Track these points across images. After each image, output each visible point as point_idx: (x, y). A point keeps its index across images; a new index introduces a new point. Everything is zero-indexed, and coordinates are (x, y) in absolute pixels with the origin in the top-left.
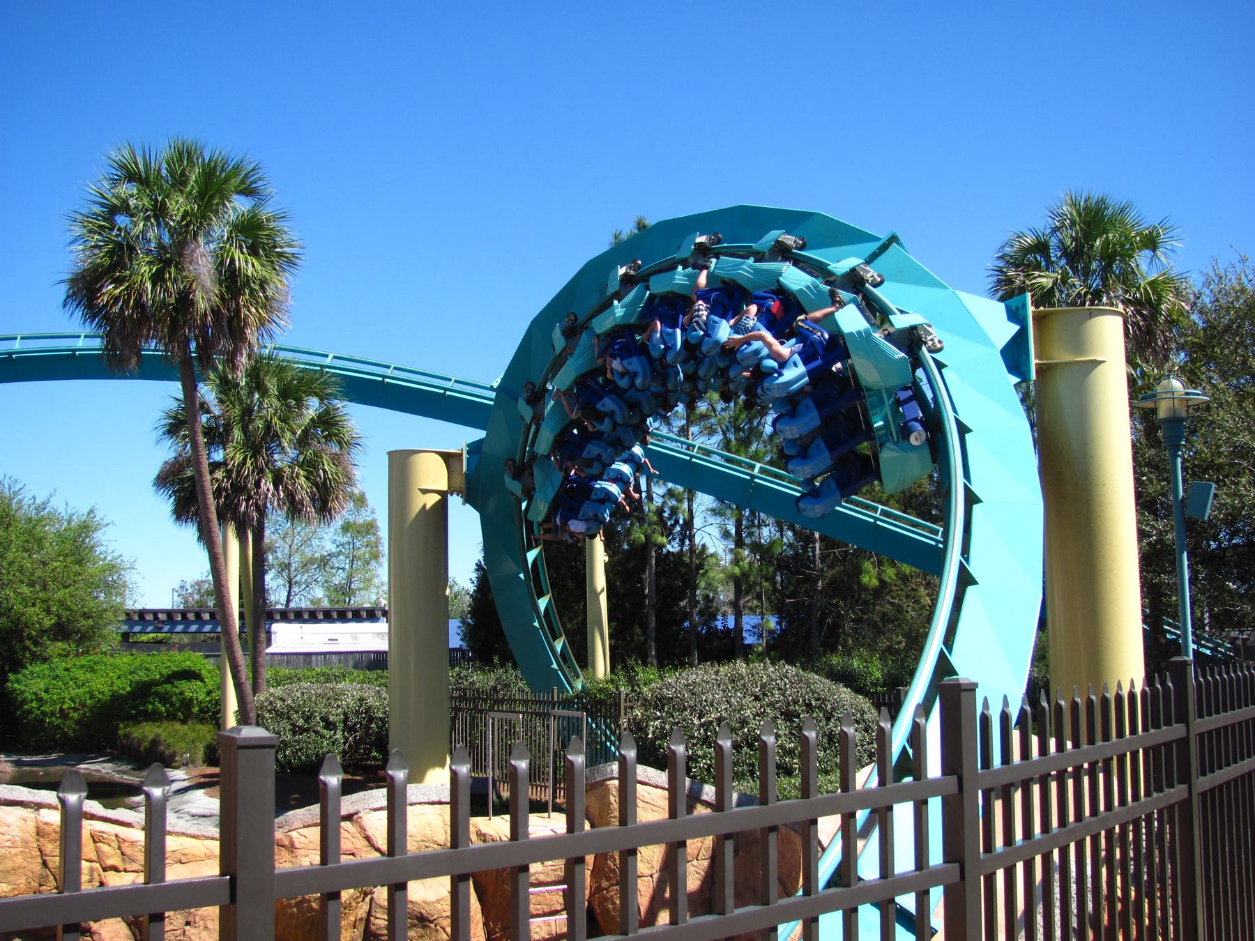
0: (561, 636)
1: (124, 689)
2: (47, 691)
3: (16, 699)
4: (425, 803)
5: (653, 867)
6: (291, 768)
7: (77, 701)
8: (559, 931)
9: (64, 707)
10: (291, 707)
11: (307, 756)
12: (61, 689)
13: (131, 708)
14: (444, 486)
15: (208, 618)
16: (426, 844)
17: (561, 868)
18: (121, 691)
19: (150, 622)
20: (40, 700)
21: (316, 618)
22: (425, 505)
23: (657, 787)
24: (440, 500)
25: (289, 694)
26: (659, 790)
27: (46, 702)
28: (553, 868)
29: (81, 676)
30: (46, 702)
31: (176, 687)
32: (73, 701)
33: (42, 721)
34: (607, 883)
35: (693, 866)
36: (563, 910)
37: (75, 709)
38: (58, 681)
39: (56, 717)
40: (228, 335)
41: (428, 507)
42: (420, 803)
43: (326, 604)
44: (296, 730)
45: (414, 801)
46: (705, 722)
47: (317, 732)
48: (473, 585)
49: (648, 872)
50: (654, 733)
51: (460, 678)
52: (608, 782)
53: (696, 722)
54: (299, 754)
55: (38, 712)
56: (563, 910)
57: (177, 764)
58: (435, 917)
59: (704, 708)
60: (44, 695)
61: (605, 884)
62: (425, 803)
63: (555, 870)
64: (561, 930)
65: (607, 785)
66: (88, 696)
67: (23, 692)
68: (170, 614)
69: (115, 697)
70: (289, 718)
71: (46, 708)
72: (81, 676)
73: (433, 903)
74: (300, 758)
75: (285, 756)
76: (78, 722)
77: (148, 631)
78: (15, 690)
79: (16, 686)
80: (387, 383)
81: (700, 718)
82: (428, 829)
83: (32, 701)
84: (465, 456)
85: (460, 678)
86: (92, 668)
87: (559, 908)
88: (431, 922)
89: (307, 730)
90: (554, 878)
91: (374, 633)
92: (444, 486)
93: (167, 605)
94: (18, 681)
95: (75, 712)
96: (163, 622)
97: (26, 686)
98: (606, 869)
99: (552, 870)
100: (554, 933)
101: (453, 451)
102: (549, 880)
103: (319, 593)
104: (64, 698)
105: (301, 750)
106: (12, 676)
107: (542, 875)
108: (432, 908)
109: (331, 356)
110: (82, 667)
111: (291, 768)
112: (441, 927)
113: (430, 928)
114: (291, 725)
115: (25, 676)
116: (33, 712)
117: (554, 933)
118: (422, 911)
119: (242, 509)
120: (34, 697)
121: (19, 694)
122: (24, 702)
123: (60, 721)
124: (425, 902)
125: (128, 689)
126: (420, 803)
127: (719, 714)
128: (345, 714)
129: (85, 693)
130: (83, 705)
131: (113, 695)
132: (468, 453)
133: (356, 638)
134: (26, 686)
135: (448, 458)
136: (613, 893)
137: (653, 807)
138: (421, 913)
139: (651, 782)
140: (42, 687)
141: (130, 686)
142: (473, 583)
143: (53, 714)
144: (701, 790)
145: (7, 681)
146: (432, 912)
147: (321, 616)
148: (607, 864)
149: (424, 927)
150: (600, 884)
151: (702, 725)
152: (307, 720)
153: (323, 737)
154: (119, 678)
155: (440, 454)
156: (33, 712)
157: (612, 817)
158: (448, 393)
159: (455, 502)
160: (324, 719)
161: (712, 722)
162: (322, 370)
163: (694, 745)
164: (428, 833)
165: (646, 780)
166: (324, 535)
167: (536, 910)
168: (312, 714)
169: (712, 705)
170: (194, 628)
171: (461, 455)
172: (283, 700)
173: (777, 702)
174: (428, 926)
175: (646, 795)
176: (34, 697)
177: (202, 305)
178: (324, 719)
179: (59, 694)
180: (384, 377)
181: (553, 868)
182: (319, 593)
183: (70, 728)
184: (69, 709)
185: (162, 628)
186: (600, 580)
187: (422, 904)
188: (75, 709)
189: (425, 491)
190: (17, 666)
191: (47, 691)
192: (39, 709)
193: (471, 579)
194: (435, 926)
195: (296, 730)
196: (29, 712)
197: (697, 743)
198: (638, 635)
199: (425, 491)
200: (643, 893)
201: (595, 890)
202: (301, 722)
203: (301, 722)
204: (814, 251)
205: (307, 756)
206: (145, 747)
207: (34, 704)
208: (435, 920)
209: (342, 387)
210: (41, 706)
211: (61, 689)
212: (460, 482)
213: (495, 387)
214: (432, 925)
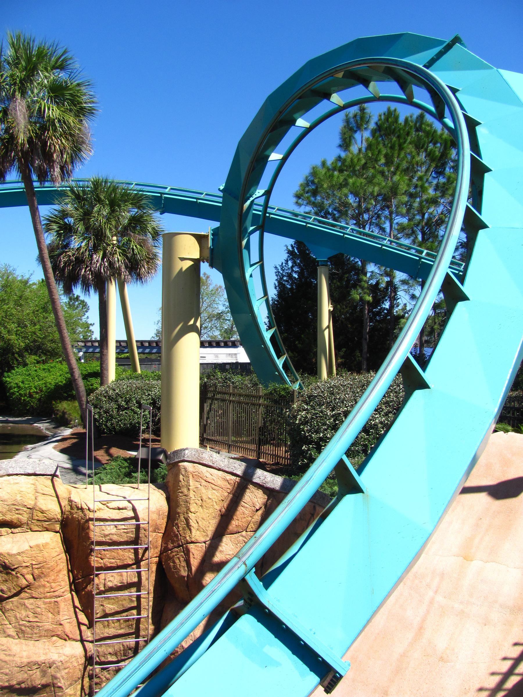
0: (285, 354)
1: (62, 382)
2: (23, 382)
3: (7, 387)
4: (22, 474)
5: (207, 536)
6: (115, 431)
7: (38, 388)
8: (130, 581)
9: (31, 391)
10: (119, 395)
11: (125, 424)
12: (30, 381)
13: (64, 392)
14: (197, 256)
15: (148, 345)
16: (17, 507)
17: (132, 531)
18: (60, 383)
19: (147, 348)
20: (19, 387)
21: (204, 345)
22: (181, 269)
23: (219, 470)
24: (192, 265)
25: (118, 387)
26: (221, 472)
27: (22, 389)
28: (126, 531)
29: (42, 374)
30: (22, 389)
31: (89, 382)
32: (36, 389)
33: (20, 399)
34: (172, 545)
35: (242, 536)
36: (133, 564)
37: (37, 393)
38: (29, 377)
39: (27, 397)
40: (41, 157)
41: (184, 269)
42: (17, 475)
43: (220, 338)
44: (120, 408)
45: (11, 473)
46: (335, 414)
47: (133, 410)
48: (266, 326)
49: (203, 539)
50: (300, 420)
51: (226, 379)
52: (180, 464)
53: (329, 413)
54: (120, 423)
55: (18, 394)
56: (133, 564)
57: (71, 426)
58: (16, 566)
59: (337, 404)
60: (21, 385)
61: (170, 546)
62: (22, 474)
63: (127, 533)
64: (131, 579)
65: (179, 466)
66: (44, 385)
67: (10, 383)
68: (150, 342)
69: (57, 386)
70: (117, 401)
71: (22, 392)
72: (42, 374)
73: (15, 555)
74: (120, 426)
75: (112, 424)
76: (39, 400)
77: (96, 351)
78: (7, 381)
79: (8, 379)
80: (199, 202)
81: (333, 410)
82: (19, 495)
83: (15, 388)
84: (210, 237)
85: (226, 379)
86: (49, 370)
87: (130, 562)
88: (13, 570)
89: (126, 409)
90: (126, 539)
91: (227, 354)
92: (197, 256)
93: (149, 339)
94: (9, 377)
95: (36, 394)
96: (124, 347)
97: (12, 379)
98: (172, 533)
99: (125, 532)
100: (125, 581)
101: (203, 233)
102: (122, 540)
103: (217, 333)
104: (31, 386)
105: (121, 420)
106: (6, 374)
107: (115, 536)
108: (13, 559)
109: (169, 188)
110: (44, 369)
111: (115, 431)
112: (21, 575)
113: (12, 575)
114: (117, 405)
115: (13, 374)
116: (15, 394)
117: (125, 581)
118: (6, 561)
119: (82, 273)
120: (15, 385)
121: (8, 384)
122: (11, 388)
123: (29, 399)
124: (8, 554)
125: (64, 382)
126: (17, 475)
127: (346, 409)
128: (153, 399)
129: (42, 384)
130: (41, 391)
131: (55, 386)
132: (213, 235)
133: (217, 357)
134: (12, 379)
135: (200, 239)
136: (174, 554)
137: (213, 486)
138: (4, 562)
139: (215, 466)
140: (21, 380)
141: (65, 380)
142: (266, 324)
143: (25, 395)
144: (253, 474)
145: (4, 376)
146: (14, 563)
147: (214, 344)
148: (173, 529)
149: (8, 573)
150: (167, 545)
151: (333, 416)
152: (127, 402)
153: (135, 413)
154: (60, 376)
155: (194, 235)
156: (15, 394)
157: (179, 492)
158: (384, 247)
159: (205, 267)
160: (138, 402)
161: (341, 414)
162: (161, 197)
163: (326, 430)
164: (19, 498)
165: (211, 464)
166: (220, 302)
167: (111, 563)
168: (130, 399)
169: (343, 402)
170: (147, 351)
171: (208, 236)
172: (114, 390)
173: (391, 402)
174: (10, 573)
175: (208, 475)
176: (15, 385)
177: (22, 138)
178: (138, 402)
179: (29, 384)
180: (197, 199)
181: (126, 531)
182: (217, 333)
183: (34, 403)
184: (33, 392)
185: (124, 350)
186: (326, 320)
187: (6, 555)
188: (37, 393)
189: (182, 259)
190: (11, 368)
191: (23, 382)
192: (18, 392)
193: (265, 322)
194: (16, 573)
195: (120, 408)
196: (13, 393)
197: (328, 429)
198: (358, 357)
199: (182, 259)
200: (195, 556)
201: (164, 549)
202: (123, 403)
203: (123, 403)
204: (436, 72)
205: (125, 424)
206: (60, 416)
207: (16, 390)
208: (16, 568)
209: (152, 199)
210: (19, 391)
211: (30, 381)
212: (207, 253)
213: (221, 189)
214: (14, 573)
